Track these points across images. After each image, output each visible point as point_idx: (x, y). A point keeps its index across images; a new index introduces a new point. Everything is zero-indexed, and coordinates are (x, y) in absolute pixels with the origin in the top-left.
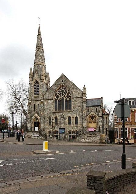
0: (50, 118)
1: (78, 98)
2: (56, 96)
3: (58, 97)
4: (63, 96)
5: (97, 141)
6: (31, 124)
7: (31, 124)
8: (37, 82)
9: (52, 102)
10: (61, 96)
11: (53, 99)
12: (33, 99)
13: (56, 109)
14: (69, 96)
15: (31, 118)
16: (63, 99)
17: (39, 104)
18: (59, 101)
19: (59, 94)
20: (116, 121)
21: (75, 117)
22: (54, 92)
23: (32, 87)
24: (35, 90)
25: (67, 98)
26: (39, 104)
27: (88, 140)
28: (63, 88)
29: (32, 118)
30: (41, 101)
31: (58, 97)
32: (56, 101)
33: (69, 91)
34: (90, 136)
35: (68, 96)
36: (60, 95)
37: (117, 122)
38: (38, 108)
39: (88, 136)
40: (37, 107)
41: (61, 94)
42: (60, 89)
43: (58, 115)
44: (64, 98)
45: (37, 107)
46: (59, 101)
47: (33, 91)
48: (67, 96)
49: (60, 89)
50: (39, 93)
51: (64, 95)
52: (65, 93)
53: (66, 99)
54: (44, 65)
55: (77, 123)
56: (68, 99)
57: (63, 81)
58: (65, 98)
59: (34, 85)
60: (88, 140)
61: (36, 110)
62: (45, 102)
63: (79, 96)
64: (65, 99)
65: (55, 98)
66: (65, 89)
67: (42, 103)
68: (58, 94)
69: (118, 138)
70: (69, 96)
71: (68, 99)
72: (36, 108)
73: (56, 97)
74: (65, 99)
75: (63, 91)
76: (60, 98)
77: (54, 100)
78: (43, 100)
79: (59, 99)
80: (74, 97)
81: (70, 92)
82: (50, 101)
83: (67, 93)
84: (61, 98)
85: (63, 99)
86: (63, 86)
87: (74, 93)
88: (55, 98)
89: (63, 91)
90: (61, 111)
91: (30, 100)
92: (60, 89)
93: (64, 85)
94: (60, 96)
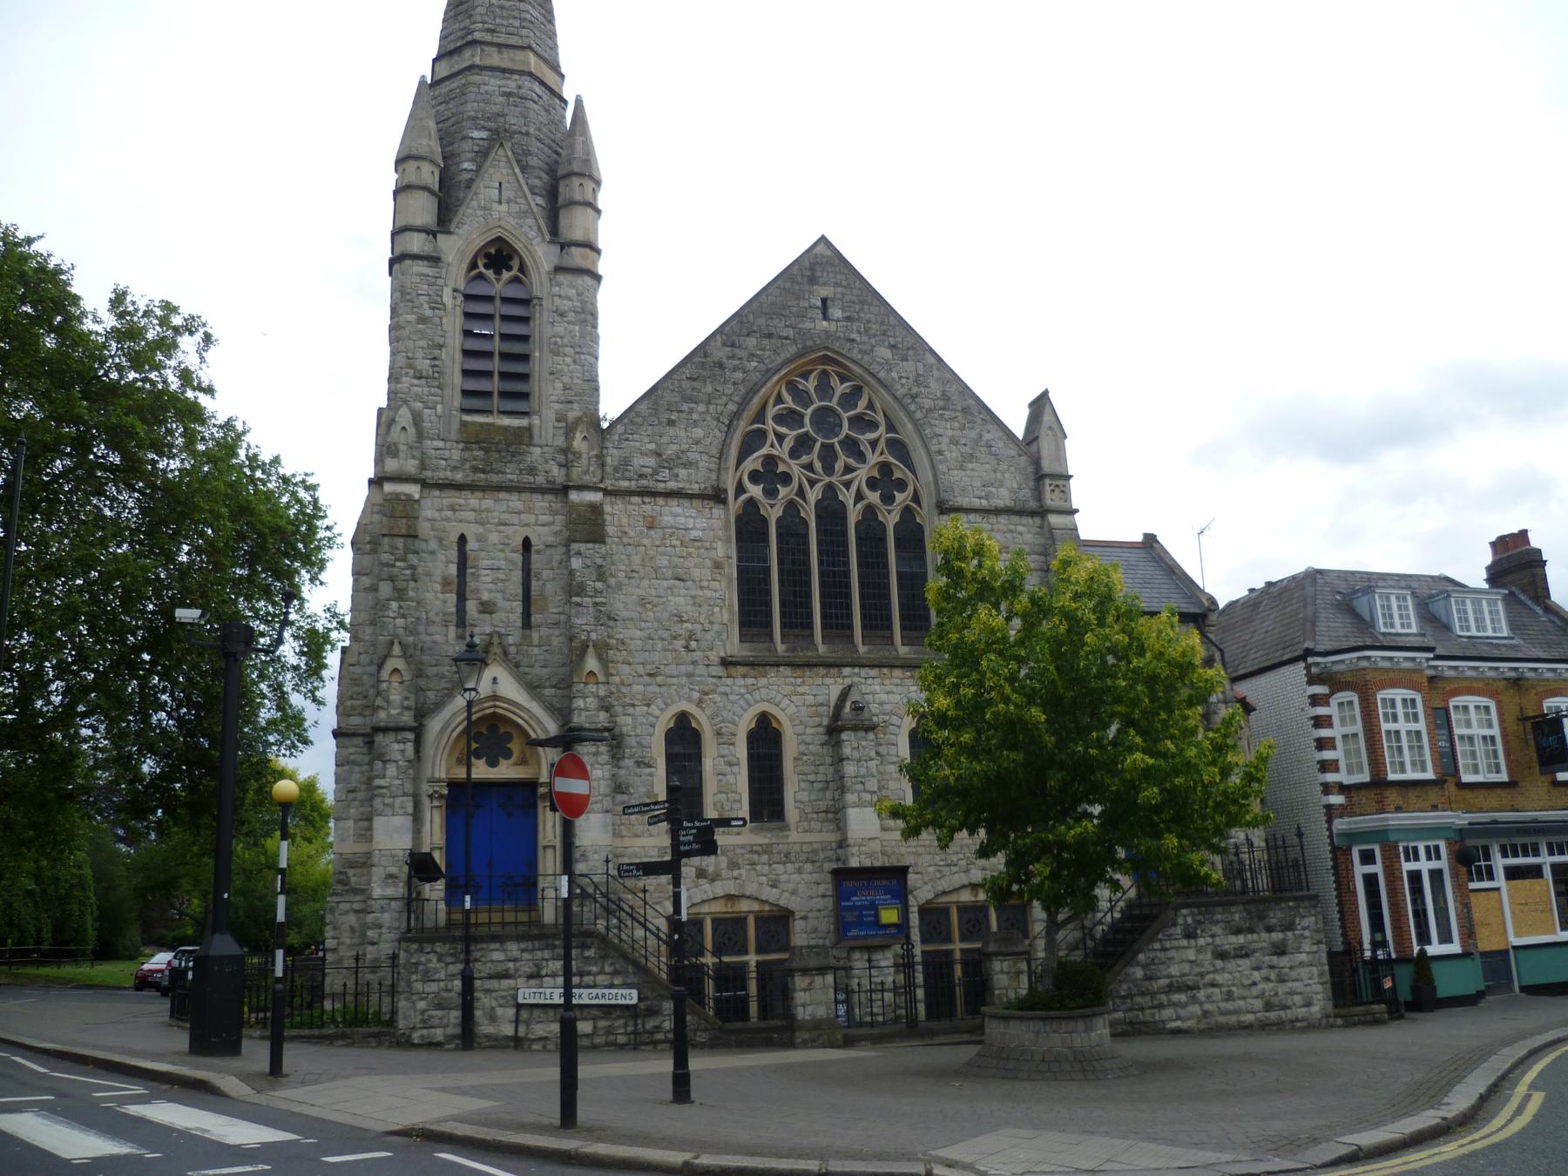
0: (684, 741)
1: (997, 512)
2: (753, 462)
3: (770, 476)
4: (829, 469)
5: (1308, 1004)
6: (417, 817)
7: (417, 817)
8: (499, 255)
9: (708, 533)
10: (809, 467)
11: (718, 497)
12: (448, 457)
13: (753, 618)
14: (901, 485)
15: (418, 731)
16: (831, 512)
17: (527, 543)
18: (792, 530)
19: (788, 443)
20: (1331, 777)
21: (746, 723)
22: (736, 416)
23: (436, 305)
24: (525, 339)
25: (874, 497)
26: (527, 543)
27: (1229, 997)
28: (824, 389)
29: (435, 725)
30: (574, 496)
31: (770, 476)
32: (749, 528)
33: (891, 427)
34: (1243, 953)
35: (885, 481)
36: (861, 457)
37: (1343, 788)
38: (516, 587)
39: (1222, 955)
40: (495, 579)
41: (803, 444)
42: (801, 396)
43: (796, 700)
44: (847, 497)
45: (495, 579)
46: (792, 530)
47: (453, 362)
48: (872, 484)
49: (792, 387)
50: (524, 396)
51: (848, 469)
52: (852, 446)
53: (752, 502)
54: (550, 77)
55: (767, 801)
56: (891, 519)
57: (836, 312)
58: (859, 497)
59: (461, 285)
60: (1229, 997)
61: (487, 608)
62: (617, 514)
63: (1003, 498)
64: (854, 514)
65: (740, 489)
66: (849, 399)
67: (589, 527)
68: (782, 451)
69: (1446, 938)
70: (901, 485)
71: (891, 519)
72: (485, 585)
73: (755, 477)
74: (854, 514)
75: (825, 419)
76: (801, 492)
77: (735, 506)
78: (595, 497)
79: (791, 507)
80: (963, 501)
81: (907, 432)
82: (677, 514)
83: (874, 444)
84: (814, 495)
85: (831, 512)
86: (826, 360)
87: (952, 454)
88: (740, 489)
89: (825, 419)
90: (781, 648)
91: (411, 466)
92: (801, 396)
93: (817, 346)
94: (795, 468)
